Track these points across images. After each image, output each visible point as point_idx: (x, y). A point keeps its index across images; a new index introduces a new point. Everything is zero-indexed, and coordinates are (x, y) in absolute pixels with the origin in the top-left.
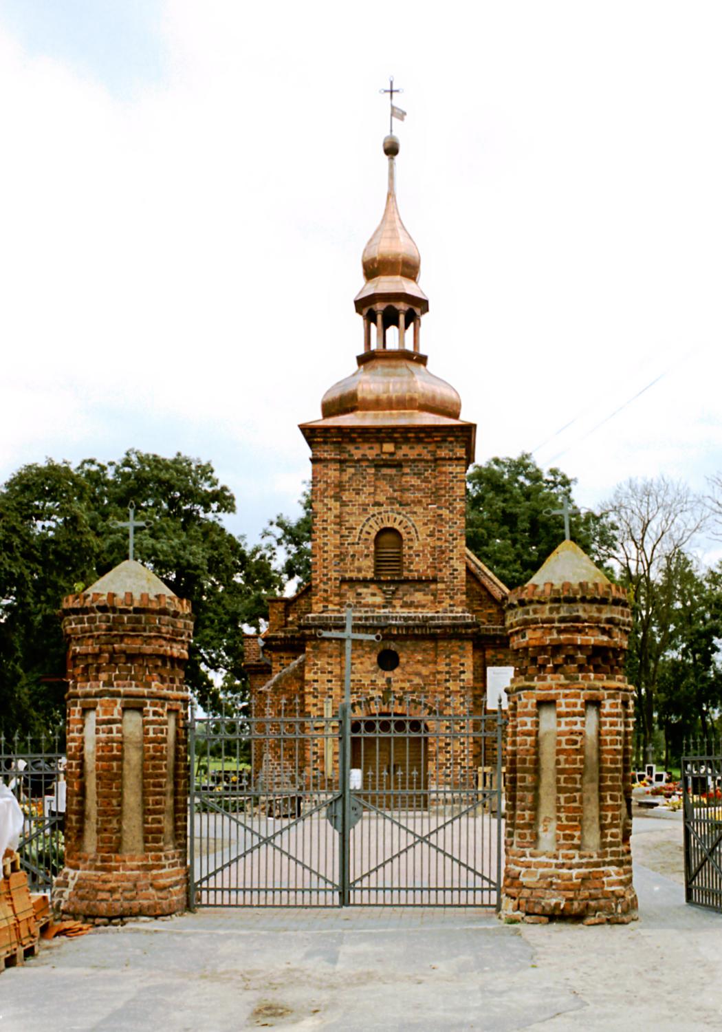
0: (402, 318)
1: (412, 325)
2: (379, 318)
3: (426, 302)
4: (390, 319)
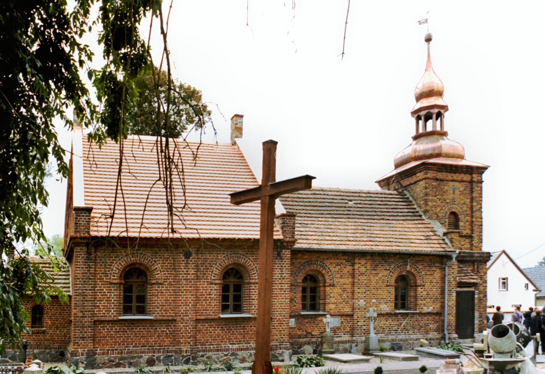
0: (434, 116)
1: (439, 119)
2: (423, 118)
3: (447, 106)
4: (428, 117)
